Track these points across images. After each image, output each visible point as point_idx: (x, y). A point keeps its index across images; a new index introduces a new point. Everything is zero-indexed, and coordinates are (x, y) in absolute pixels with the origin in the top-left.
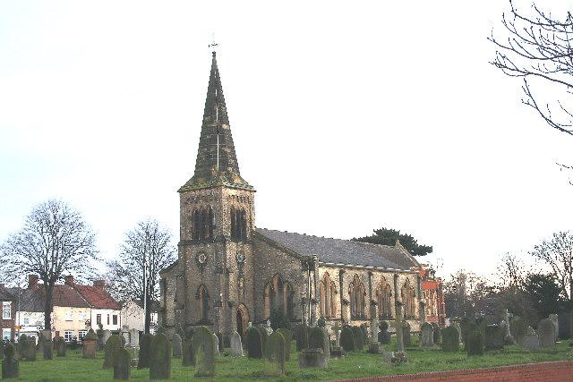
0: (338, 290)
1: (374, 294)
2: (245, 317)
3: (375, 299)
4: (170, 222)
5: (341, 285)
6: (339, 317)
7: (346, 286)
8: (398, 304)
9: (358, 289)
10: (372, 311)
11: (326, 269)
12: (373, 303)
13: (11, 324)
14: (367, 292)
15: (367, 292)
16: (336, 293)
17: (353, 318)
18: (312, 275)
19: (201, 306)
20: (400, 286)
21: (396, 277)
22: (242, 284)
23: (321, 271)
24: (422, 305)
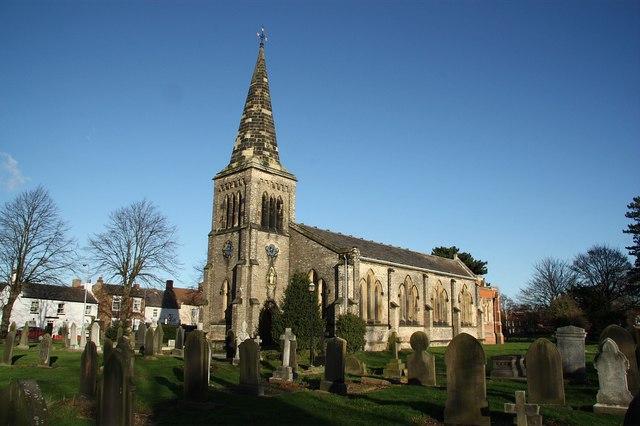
0: (385, 291)
1: (428, 298)
2: (50, 306)
3: (429, 304)
4: (196, 287)
5: (389, 285)
6: (386, 322)
7: (394, 286)
8: (455, 310)
9: (409, 293)
10: (426, 316)
11: (370, 266)
12: (427, 308)
13: (141, 316)
14: (421, 296)
15: (421, 296)
16: (382, 294)
17: (402, 324)
18: (350, 270)
19: (316, 246)
20: (457, 292)
21: (453, 281)
22: (271, 278)
23: (364, 268)
24: (479, 312)
